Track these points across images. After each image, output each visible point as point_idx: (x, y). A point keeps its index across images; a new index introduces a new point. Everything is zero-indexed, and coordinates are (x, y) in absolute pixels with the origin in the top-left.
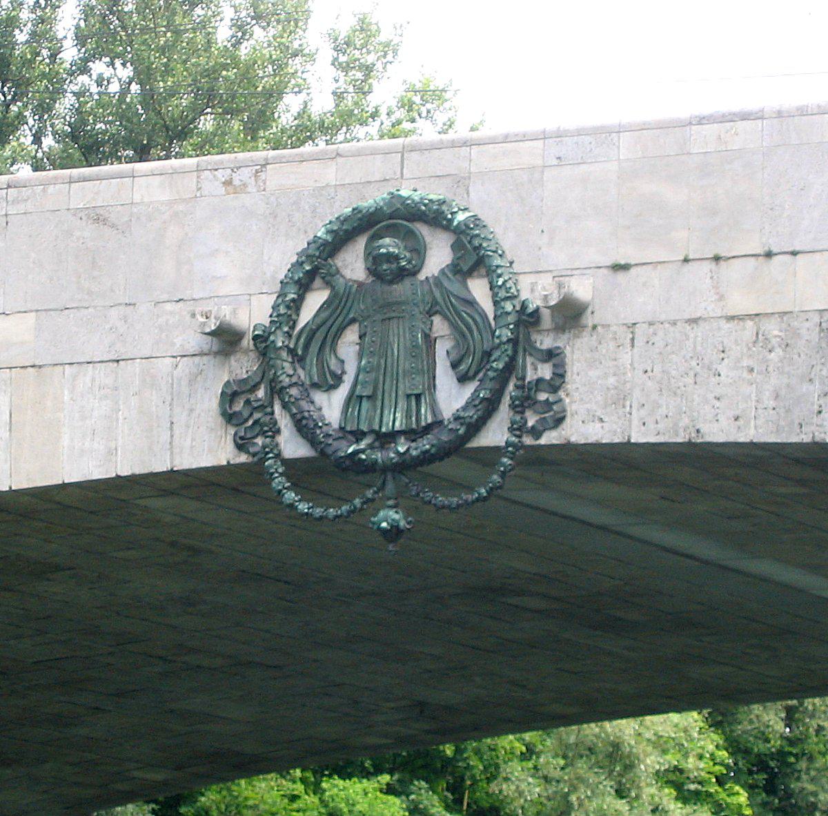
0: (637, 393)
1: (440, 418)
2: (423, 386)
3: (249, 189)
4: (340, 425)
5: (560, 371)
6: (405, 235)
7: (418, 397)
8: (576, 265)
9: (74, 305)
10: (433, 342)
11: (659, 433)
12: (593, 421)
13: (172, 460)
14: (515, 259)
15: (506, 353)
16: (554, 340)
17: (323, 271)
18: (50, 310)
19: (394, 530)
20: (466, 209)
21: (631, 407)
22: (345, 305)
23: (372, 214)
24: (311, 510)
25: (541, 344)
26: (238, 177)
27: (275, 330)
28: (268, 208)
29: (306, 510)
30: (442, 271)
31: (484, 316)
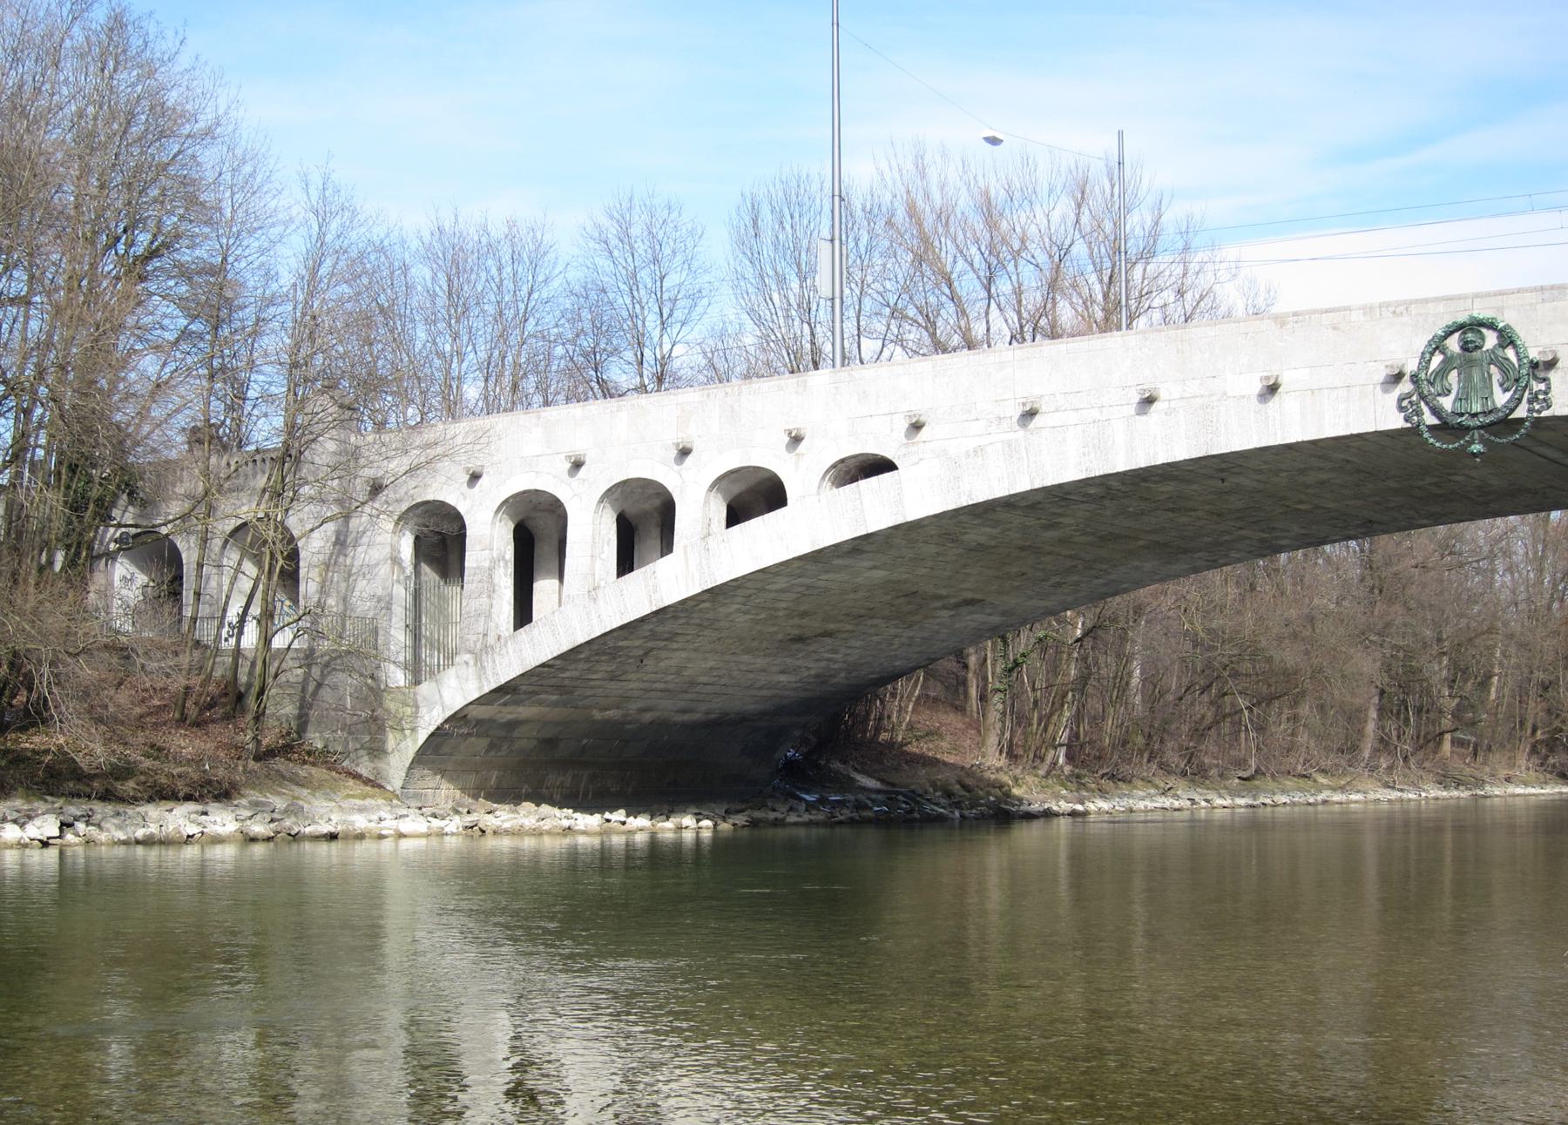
30: (1494, 347)
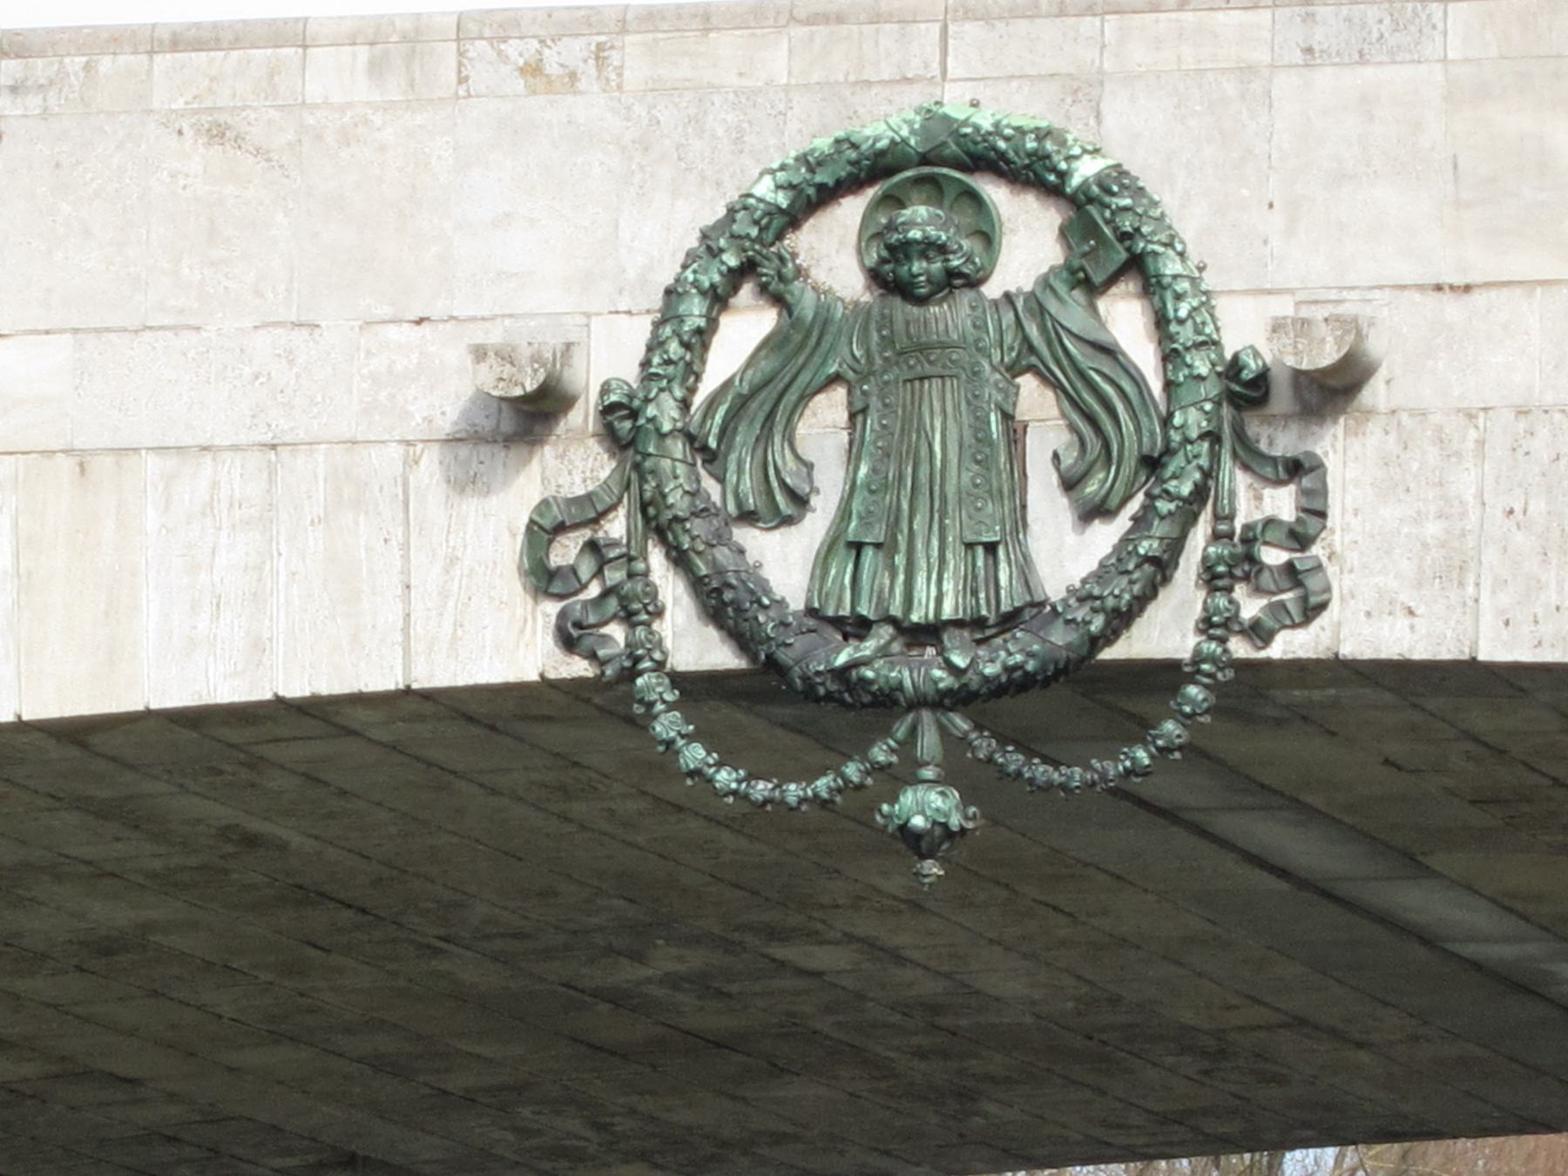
0: (1491, 556)
1: (1038, 598)
2: (1003, 529)
3: (582, 85)
4: (809, 600)
5: (1316, 505)
6: (956, 199)
7: (991, 548)
8: (1351, 279)
9: (166, 322)
10: (1020, 431)
11: (1540, 643)
12: (1390, 613)
13: (407, 668)
14: (1207, 261)
15: (1194, 463)
16: (1300, 437)
17: (765, 271)
18: (108, 330)
19: (938, 831)
20: (1096, 151)
21: (1477, 585)
22: (818, 343)
23: (882, 153)
24: (744, 785)
25: (1271, 444)
26: (556, 59)
27: (657, 394)
28: (628, 128)
29: (734, 785)
31: (1138, 381)
